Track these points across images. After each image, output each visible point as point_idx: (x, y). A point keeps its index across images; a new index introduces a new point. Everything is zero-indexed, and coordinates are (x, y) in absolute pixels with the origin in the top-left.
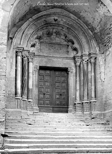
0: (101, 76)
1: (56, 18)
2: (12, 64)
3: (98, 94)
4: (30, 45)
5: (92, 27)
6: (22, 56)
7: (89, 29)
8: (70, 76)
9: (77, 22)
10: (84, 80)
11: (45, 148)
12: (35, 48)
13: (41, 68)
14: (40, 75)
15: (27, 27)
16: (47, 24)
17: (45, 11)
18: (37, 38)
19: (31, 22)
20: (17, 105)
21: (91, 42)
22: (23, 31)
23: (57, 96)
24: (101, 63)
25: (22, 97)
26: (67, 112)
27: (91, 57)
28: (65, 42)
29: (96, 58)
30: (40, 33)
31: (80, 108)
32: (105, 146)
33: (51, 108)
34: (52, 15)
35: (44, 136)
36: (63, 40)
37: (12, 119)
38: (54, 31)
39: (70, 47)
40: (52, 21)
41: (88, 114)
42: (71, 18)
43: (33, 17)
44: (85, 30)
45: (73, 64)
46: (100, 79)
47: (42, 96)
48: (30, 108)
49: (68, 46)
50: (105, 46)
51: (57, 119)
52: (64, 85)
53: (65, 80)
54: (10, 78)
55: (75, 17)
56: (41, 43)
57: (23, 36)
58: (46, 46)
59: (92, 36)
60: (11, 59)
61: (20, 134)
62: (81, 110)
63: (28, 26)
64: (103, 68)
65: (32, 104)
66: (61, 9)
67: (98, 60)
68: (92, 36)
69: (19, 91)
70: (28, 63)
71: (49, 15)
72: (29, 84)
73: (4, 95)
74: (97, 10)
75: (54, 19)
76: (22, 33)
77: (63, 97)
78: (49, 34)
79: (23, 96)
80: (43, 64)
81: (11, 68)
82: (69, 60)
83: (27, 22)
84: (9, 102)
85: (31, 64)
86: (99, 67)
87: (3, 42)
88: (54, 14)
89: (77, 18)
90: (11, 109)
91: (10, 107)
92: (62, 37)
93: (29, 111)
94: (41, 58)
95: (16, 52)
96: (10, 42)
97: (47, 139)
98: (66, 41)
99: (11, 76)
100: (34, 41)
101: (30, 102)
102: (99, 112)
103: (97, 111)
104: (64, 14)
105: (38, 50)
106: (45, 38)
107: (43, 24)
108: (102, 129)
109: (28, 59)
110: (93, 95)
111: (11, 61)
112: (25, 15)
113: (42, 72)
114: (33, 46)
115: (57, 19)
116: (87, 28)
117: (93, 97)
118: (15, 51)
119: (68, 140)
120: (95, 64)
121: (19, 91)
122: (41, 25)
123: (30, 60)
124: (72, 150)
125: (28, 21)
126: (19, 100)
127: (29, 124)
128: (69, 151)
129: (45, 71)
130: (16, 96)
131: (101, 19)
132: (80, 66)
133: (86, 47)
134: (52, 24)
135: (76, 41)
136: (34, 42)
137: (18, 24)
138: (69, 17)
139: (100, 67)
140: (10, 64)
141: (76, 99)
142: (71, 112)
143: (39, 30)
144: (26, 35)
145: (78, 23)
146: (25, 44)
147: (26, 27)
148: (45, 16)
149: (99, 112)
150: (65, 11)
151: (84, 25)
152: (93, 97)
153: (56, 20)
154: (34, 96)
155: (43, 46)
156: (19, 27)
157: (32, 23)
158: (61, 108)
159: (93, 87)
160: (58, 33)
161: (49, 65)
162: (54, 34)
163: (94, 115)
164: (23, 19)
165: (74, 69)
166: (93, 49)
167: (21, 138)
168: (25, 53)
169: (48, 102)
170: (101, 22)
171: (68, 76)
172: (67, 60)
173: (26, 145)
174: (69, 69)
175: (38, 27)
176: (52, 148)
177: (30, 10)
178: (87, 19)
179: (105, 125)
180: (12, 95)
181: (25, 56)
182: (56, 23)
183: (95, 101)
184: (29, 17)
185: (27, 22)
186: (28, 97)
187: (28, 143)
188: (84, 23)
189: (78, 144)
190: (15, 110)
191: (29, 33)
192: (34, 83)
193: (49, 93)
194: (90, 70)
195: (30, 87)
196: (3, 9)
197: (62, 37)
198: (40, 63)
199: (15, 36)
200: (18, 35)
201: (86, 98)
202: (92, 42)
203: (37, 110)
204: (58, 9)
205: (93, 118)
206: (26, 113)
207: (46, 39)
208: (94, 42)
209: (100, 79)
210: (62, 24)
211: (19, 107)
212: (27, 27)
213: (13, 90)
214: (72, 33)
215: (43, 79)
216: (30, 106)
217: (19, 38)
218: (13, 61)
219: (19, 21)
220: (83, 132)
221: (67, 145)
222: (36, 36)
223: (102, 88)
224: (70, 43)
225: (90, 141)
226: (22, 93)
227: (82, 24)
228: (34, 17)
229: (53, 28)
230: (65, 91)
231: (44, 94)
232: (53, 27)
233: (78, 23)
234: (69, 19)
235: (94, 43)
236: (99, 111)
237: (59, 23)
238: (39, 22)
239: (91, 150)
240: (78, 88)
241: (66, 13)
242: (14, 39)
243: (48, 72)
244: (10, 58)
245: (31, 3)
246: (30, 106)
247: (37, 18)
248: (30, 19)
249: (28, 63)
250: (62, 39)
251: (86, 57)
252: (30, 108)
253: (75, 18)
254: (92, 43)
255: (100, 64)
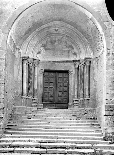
0: (94, 77)
1: (57, 29)
2: (19, 70)
3: (91, 93)
4: (36, 53)
5: (88, 34)
6: (29, 63)
7: (85, 36)
8: (70, 77)
9: (74, 31)
10: (81, 80)
11: (32, 138)
12: (41, 55)
13: (46, 71)
14: (45, 76)
15: (31, 39)
16: (50, 34)
17: (46, 24)
18: (43, 46)
19: (35, 34)
20: (22, 103)
21: (86, 48)
22: (28, 43)
23: (60, 94)
24: (95, 66)
25: (28, 96)
26: (67, 109)
27: (86, 61)
28: (66, 48)
29: (90, 62)
30: (44, 42)
31: (77, 104)
32: (81, 138)
33: (54, 104)
34: (52, 27)
35: (35, 129)
36: (64, 46)
37: (17, 115)
38: (57, 39)
39: (70, 52)
40: (53, 32)
41: (82, 110)
42: (69, 28)
43: (36, 30)
44: (81, 37)
45: (73, 66)
46: (94, 79)
47: (46, 94)
48: (35, 105)
49: (69, 51)
50: (98, 51)
51: (55, 114)
52: (66, 84)
53: (67, 80)
54: (18, 81)
55: (72, 27)
56: (45, 50)
57: (28, 47)
58: (50, 52)
59: (87, 43)
60: (18, 66)
61: (18, 127)
62: (78, 106)
63: (32, 38)
64: (96, 70)
65: (37, 101)
66: (60, 21)
67: (92, 63)
68: (87, 43)
69: (25, 91)
70: (34, 67)
71: (50, 27)
72: (35, 85)
73: (3, 98)
74: (88, 21)
75: (55, 30)
76: (27, 44)
77: (64, 95)
78: (53, 42)
79: (29, 96)
80: (47, 68)
81: (19, 73)
82: (69, 64)
83: (31, 35)
84: (16, 101)
85: (36, 68)
86: (92, 69)
87: (3, 57)
88: (54, 26)
89: (74, 28)
90: (18, 106)
91: (17, 105)
92: (64, 44)
93: (34, 107)
94: (45, 63)
95: (23, 60)
96: (18, 52)
97: (38, 131)
98: (67, 47)
99: (18, 80)
100: (39, 48)
101: (34, 100)
102: (91, 108)
103: (90, 107)
104: (62, 26)
105: (45, 56)
106: (49, 46)
107: (45, 35)
108: (87, 124)
109: (34, 64)
110: (87, 94)
111: (18, 68)
112: (30, 29)
113: (47, 74)
114: (39, 53)
115: (58, 30)
116: (82, 35)
117: (87, 96)
118: (21, 60)
119: (53, 132)
120: (90, 66)
121: (25, 91)
122: (44, 36)
123: (36, 65)
124: (52, 141)
125: (32, 34)
126: (30, 100)
127: (29, 119)
128: (50, 141)
129: (49, 74)
130: (22, 96)
131: (92, 28)
132: (78, 69)
133: (83, 52)
134: (54, 34)
135: (75, 46)
136: (39, 50)
137: (24, 37)
138: (67, 27)
139: (93, 70)
140: (18, 70)
141: (74, 97)
142: (70, 108)
143: (42, 40)
144: (32, 45)
145: (75, 32)
146: (31, 53)
147: (31, 39)
148: (47, 29)
149: (91, 108)
150: (63, 22)
151: (80, 33)
152: (87, 96)
153: (56, 30)
154: (39, 94)
155: (47, 53)
156: (25, 39)
157: (36, 35)
158: (63, 104)
159: (87, 87)
160: (60, 41)
161: (52, 69)
162: (57, 42)
163: (87, 110)
164: (29, 32)
165: (74, 71)
166: (88, 54)
167: (18, 130)
168: (31, 60)
169: (51, 99)
170: (93, 31)
171: (69, 77)
172: (68, 64)
173: (19, 135)
174: (69, 71)
175: (42, 37)
176: (38, 138)
177: (33, 24)
178: (82, 28)
179: (93, 120)
180: (18, 95)
181: (31, 63)
182: (57, 33)
183: (89, 98)
184: (33, 30)
185: (31, 35)
186: (33, 96)
187: (21, 134)
188: (80, 32)
189: (59, 136)
190: (21, 107)
191: (34, 43)
192: (40, 84)
193: (52, 92)
194: (85, 72)
195: (36, 88)
196: (3, 32)
197: (64, 44)
198: (44, 67)
199: (22, 47)
200: (24, 46)
201: (81, 96)
202: (87, 47)
203: (41, 106)
204: (57, 21)
205: (86, 114)
206: (30, 109)
207: (49, 46)
208: (89, 48)
209: (94, 79)
210: (62, 33)
211: (24, 104)
212: (31, 39)
213: (20, 91)
214: (71, 40)
215: (47, 80)
216: (35, 103)
217: (25, 49)
218: (20, 67)
219: (25, 35)
220: (70, 125)
221: (50, 137)
222: (41, 45)
223: (95, 87)
224: (71, 49)
225: (71, 134)
226: (28, 93)
227: (78, 33)
228: (37, 30)
229: (55, 37)
230: (66, 89)
231: (49, 93)
232: (55, 36)
233: (75, 32)
234: (67, 29)
235: (89, 48)
236: (91, 107)
237: (59, 33)
238: (41, 33)
239: (67, 141)
240: (76, 87)
241: (65, 24)
242: (20, 50)
243: (52, 74)
244: (18, 65)
245: (33, 20)
246: (35, 103)
247: (39, 31)
248: (34, 32)
249: (34, 67)
250: (64, 45)
251: (82, 61)
252: (35, 105)
253: (72, 28)
254: (87, 49)
255: (94, 67)
